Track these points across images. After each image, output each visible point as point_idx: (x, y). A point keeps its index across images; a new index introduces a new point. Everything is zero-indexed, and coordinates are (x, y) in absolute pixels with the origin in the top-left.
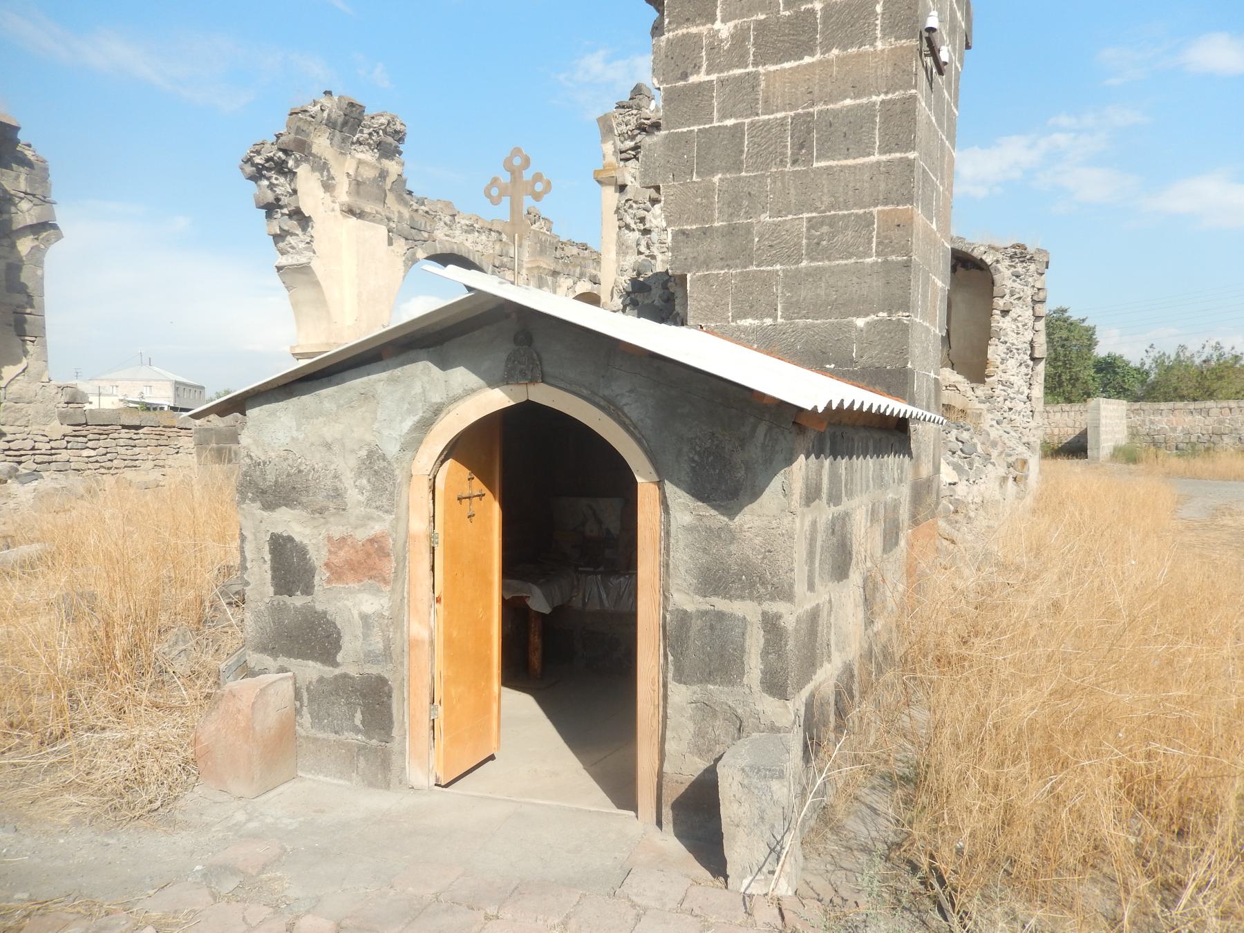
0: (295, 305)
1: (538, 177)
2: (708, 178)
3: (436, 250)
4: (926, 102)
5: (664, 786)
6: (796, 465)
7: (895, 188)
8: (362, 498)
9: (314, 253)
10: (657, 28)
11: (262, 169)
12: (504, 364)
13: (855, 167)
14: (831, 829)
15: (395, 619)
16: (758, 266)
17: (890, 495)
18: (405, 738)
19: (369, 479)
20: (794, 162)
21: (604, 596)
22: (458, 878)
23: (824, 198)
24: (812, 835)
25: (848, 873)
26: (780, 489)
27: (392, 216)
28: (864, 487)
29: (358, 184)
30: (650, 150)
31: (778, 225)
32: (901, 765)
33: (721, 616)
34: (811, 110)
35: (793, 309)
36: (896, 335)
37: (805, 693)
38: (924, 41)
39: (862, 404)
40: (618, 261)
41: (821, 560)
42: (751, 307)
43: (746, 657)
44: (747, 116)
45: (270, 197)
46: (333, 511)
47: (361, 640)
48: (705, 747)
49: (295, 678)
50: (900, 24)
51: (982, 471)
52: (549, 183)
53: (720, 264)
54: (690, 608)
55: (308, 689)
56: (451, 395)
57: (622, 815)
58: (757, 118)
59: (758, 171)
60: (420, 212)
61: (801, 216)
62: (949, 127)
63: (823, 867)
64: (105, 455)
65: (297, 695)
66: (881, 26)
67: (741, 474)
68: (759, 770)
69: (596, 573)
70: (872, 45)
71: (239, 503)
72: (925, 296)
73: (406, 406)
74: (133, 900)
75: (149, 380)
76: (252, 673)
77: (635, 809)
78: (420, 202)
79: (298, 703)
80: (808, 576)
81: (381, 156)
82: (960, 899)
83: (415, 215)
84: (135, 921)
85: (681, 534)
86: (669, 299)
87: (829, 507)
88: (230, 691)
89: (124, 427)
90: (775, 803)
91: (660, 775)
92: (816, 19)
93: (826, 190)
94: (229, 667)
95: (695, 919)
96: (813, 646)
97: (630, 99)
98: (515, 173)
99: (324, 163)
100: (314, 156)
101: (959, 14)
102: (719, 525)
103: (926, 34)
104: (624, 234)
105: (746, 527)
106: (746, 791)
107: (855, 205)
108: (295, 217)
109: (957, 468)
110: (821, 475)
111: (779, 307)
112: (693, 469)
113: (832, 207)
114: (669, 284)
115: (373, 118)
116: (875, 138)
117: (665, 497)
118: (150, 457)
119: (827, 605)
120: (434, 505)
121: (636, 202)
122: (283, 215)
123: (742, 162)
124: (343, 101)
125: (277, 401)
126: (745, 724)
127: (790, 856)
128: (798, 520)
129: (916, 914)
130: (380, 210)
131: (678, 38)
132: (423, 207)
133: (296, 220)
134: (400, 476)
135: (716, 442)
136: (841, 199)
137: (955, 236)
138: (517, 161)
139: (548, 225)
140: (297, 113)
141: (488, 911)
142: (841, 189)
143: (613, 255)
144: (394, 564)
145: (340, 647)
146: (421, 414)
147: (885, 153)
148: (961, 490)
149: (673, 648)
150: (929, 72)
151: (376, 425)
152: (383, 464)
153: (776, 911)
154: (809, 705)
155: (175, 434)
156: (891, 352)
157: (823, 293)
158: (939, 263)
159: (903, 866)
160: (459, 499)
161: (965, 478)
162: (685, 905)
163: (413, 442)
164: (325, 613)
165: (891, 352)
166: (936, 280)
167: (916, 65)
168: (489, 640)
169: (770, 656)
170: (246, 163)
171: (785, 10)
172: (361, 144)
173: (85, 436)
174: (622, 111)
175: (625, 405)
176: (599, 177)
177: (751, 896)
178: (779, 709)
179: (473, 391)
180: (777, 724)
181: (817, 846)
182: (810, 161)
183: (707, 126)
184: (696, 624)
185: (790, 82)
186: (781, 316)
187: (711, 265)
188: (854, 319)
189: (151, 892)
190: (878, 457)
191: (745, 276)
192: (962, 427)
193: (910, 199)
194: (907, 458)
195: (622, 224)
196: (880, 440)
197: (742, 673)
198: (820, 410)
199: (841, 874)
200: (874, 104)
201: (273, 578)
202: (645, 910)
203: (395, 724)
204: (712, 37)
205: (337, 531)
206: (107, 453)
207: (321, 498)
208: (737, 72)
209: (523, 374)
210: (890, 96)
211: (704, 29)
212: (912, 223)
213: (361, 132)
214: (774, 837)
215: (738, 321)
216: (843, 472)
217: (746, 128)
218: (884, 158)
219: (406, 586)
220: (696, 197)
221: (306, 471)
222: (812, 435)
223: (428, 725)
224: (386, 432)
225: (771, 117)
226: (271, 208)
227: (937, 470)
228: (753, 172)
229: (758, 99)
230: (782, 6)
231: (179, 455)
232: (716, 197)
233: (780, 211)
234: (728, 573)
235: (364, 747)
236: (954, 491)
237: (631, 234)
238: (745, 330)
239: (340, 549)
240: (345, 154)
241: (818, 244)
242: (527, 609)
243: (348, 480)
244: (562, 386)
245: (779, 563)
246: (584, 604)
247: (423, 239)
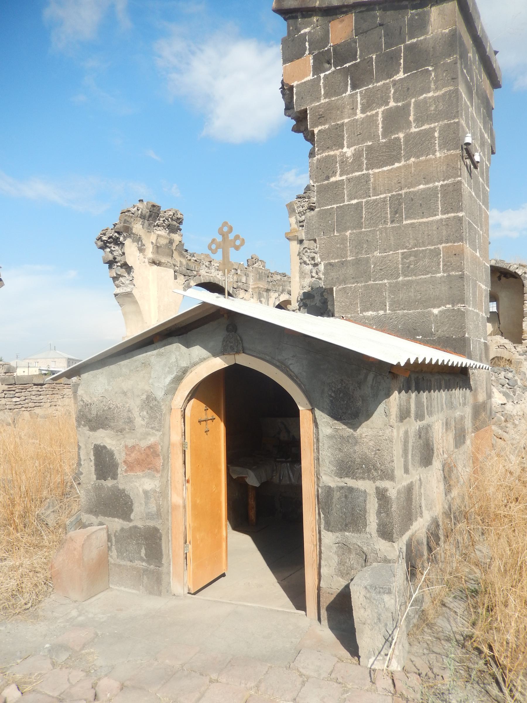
0: (124, 314)
1: (237, 237)
2: (343, 233)
3: (201, 281)
4: (468, 184)
5: (321, 596)
6: (392, 398)
7: (452, 233)
8: (144, 423)
9: (134, 285)
10: (312, 153)
11: (107, 243)
12: (221, 343)
13: (428, 223)
14: (427, 625)
15: (163, 493)
16: (374, 281)
17: (458, 413)
18: (170, 564)
19: (147, 412)
20: (392, 222)
21: (291, 475)
22: (195, 655)
23: (411, 241)
24: (415, 629)
25: (438, 656)
26: (383, 412)
27: (176, 264)
28: (440, 409)
29: (158, 247)
30: (310, 220)
31: (384, 257)
32: (473, 582)
33: (351, 490)
34: (400, 192)
35: (396, 305)
36: (457, 318)
37: (406, 537)
38: (464, 150)
39: (431, 360)
40: (300, 282)
41: (412, 454)
42: (371, 305)
43: (367, 515)
44: (364, 198)
45: (111, 257)
46: (127, 430)
47: (144, 505)
48: (345, 571)
49: (107, 529)
50: (449, 142)
51: (522, 396)
52: (243, 240)
53: (352, 281)
54: (332, 485)
55: (115, 535)
56: (192, 362)
57: (298, 613)
58: (369, 198)
59: (371, 228)
60: (192, 260)
61: (397, 252)
62: (484, 198)
63: (421, 651)
64: (25, 400)
65: (109, 539)
66: (438, 144)
67: (360, 403)
68: (376, 588)
69: (286, 462)
70: (434, 154)
71: (77, 427)
72: (474, 294)
73: (167, 369)
74: (8, 666)
75: (54, 358)
76: (84, 526)
77: (305, 611)
78: (192, 255)
79: (109, 544)
80: (404, 464)
81: (170, 232)
82: (510, 676)
83: (189, 262)
84: (7, 680)
85: (326, 440)
86: (325, 302)
87: (417, 422)
88: (70, 537)
89: (35, 385)
90: (387, 609)
91: (319, 588)
92: (401, 142)
93: (411, 237)
94: (71, 522)
95: (339, 685)
96: (409, 508)
97: (304, 193)
98: (224, 235)
99: (140, 238)
100: (134, 234)
101: (486, 135)
102: (348, 434)
103: (465, 147)
104: (304, 267)
105: (364, 435)
106: (369, 601)
107: (429, 244)
108: (124, 267)
109: (505, 394)
110: (409, 403)
111: (387, 304)
112: (331, 401)
113: (416, 246)
114: (324, 293)
115: (165, 212)
116: (438, 206)
117: (315, 418)
118: (49, 401)
119: (418, 482)
120: (185, 426)
121: (309, 249)
122: (118, 266)
123: (362, 223)
124: (149, 204)
125: (97, 369)
126: (368, 557)
127: (399, 644)
128: (395, 431)
129: (482, 685)
130: (169, 260)
131: (323, 158)
132: (193, 258)
133: (125, 269)
134: (165, 410)
135: (344, 385)
136: (421, 241)
137: (498, 259)
138: (225, 229)
139: (263, 264)
140: (125, 212)
141: (212, 677)
142: (420, 235)
143: (297, 279)
144: (162, 461)
145: (133, 510)
146: (176, 374)
147: (445, 214)
148: (509, 407)
149: (323, 509)
150: (469, 168)
151: (151, 381)
152: (155, 403)
153: (391, 681)
154: (409, 545)
155: (62, 388)
156: (455, 328)
157: (412, 295)
158: (483, 275)
159: (473, 652)
160: (199, 422)
161: (511, 400)
162: (333, 676)
163: (172, 390)
164: (124, 490)
165: (455, 328)
166: (481, 285)
167: (460, 164)
168: (220, 504)
169: (382, 515)
170: (98, 240)
171: (382, 139)
172: (159, 226)
173: (14, 391)
174: (300, 200)
175: (290, 364)
176: (288, 236)
177: (374, 670)
178: (389, 548)
179: (205, 359)
180: (388, 558)
181: (418, 637)
182: (401, 220)
183: (341, 205)
184: (337, 495)
185: (388, 178)
186: (389, 309)
187: (347, 282)
188: (432, 309)
189: (19, 661)
190: (448, 390)
191: (367, 287)
192: (508, 370)
193: (461, 239)
194: (468, 391)
195: (302, 261)
196: (449, 380)
197: (365, 525)
198: (402, 364)
199: (433, 656)
200: (437, 187)
201: (96, 470)
202: (308, 678)
203: (164, 556)
204: (342, 156)
205: (130, 442)
206: (26, 399)
207: (121, 423)
208: (357, 174)
209: (232, 349)
210: (446, 182)
211: (337, 152)
212: (463, 252)
213: (159, 220)
214: (387, 632)
215: (364, 313)
216: (425, 400)
217: (364, 204)
218: (444, 216)
219: (169, 473)
220: (337, 244)
221: (113, 408)
222: (402, 379)
223: (182, 556)
224: (156, 385)
225: (378, 197)
226: (111, 263)
227: (489, 396)
228: (369, 228)
229: (370, 188)
230: (381, 137)
231: (64, 399)
232: (348, 243)
233: (385, 250)
234: (354, 463)
235: (147, 570)
236: (504, 408)
237: (307, 267)
238: (368, 318)
239: (132, 452)
240: (151, 232)
241: (408, 267)
242: (247, 485)
243: (136, 412)
244: (255, 355)
245: (385, 457)
246: (280, 480)
247: (193, 275)
